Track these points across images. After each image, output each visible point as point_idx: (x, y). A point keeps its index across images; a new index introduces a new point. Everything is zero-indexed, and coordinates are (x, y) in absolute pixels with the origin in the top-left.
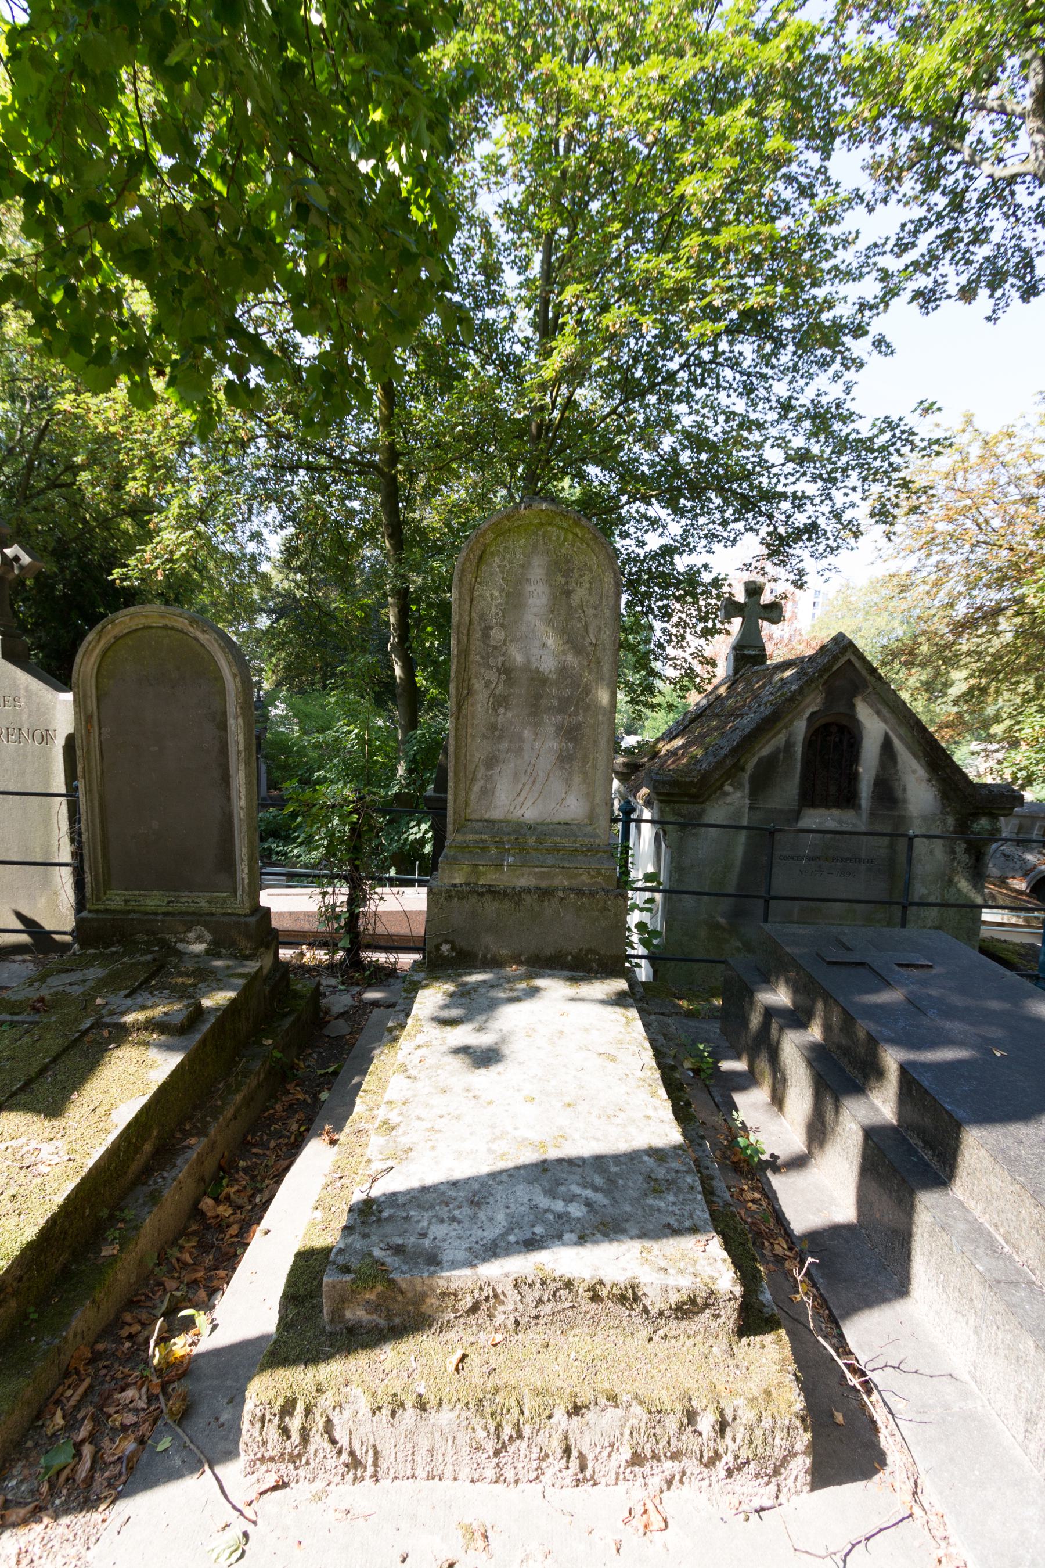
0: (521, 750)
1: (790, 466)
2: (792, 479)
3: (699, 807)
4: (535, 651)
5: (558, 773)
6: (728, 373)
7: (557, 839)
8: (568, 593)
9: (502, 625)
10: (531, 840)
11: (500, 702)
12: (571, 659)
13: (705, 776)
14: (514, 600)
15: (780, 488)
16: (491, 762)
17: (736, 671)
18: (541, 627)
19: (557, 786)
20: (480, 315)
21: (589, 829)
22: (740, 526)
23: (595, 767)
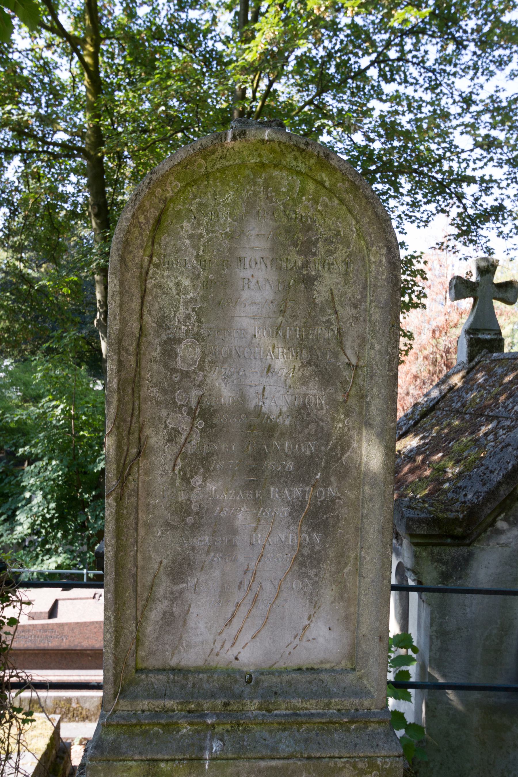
0: (231, 547)
1: (478, 151)
2: (480, 164)
3: (465, 550)
4: (255, 379)
5: (297, 584)
6: (413, 71)
7: (297, 702)
8: (309, 281)
9: (197, 337)
10: (252, 706)
11: (195, 464)
12: (314, 392)
13: (473, 513)
14: (217, 290)
15: (469, 172)
16: (180, 569)
17: (471, 357)
18: (264, 339)
19: (294, 606)
20: (183, 15)
21: (351, 678)
22: (432, 207)
23: (358, 571)
